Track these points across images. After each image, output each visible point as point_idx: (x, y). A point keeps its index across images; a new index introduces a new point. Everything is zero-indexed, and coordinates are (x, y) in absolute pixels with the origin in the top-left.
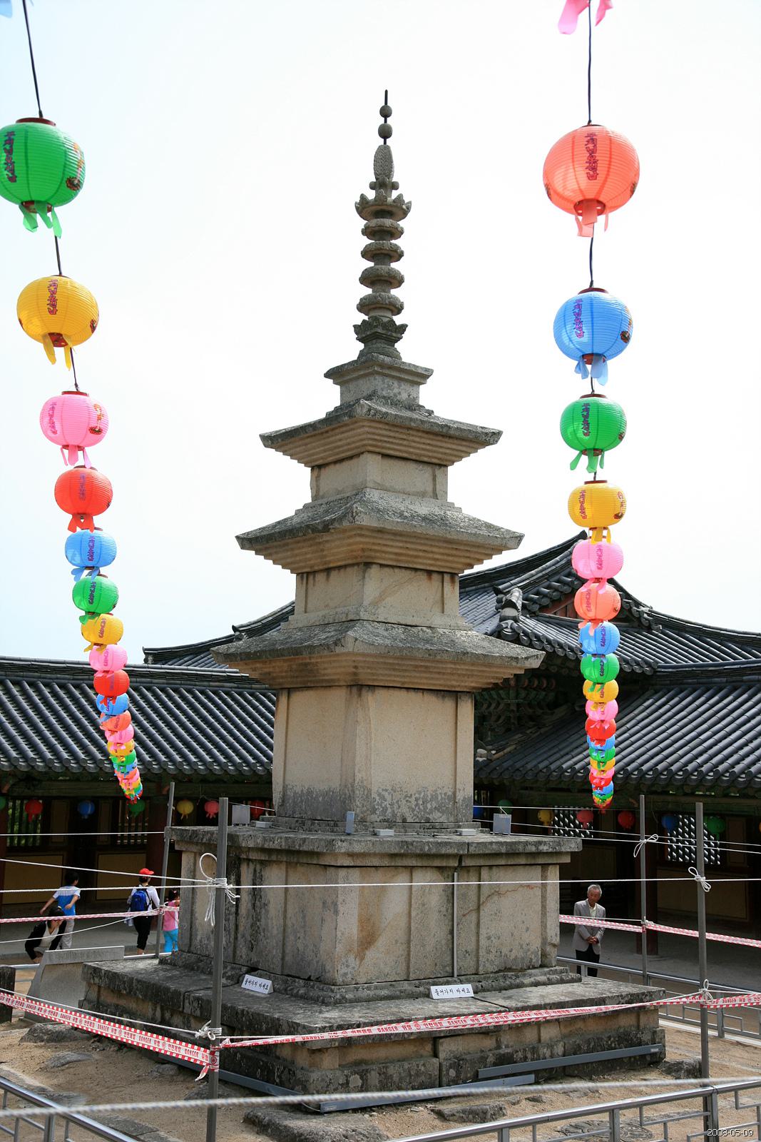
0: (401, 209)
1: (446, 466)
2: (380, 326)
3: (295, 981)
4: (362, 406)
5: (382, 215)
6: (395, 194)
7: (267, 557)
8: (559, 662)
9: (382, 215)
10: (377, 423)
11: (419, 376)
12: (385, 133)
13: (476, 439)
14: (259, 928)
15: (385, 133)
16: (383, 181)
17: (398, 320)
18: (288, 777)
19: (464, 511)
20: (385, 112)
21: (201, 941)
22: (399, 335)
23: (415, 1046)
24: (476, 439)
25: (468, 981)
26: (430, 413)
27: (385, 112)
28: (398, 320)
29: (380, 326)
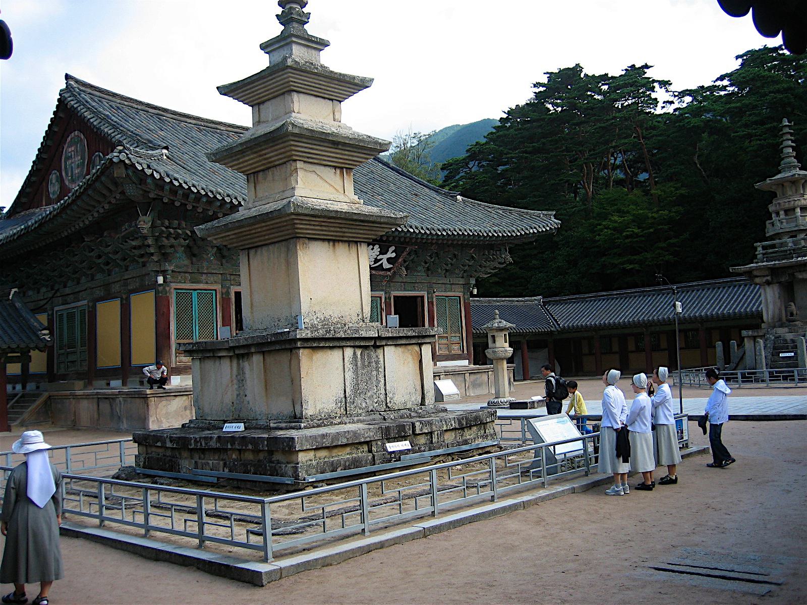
1: (340, 102)
13: (353, 85)
17: (305, 10)
18: (341, 353)
24: (353, 85)
28: (305, 10)
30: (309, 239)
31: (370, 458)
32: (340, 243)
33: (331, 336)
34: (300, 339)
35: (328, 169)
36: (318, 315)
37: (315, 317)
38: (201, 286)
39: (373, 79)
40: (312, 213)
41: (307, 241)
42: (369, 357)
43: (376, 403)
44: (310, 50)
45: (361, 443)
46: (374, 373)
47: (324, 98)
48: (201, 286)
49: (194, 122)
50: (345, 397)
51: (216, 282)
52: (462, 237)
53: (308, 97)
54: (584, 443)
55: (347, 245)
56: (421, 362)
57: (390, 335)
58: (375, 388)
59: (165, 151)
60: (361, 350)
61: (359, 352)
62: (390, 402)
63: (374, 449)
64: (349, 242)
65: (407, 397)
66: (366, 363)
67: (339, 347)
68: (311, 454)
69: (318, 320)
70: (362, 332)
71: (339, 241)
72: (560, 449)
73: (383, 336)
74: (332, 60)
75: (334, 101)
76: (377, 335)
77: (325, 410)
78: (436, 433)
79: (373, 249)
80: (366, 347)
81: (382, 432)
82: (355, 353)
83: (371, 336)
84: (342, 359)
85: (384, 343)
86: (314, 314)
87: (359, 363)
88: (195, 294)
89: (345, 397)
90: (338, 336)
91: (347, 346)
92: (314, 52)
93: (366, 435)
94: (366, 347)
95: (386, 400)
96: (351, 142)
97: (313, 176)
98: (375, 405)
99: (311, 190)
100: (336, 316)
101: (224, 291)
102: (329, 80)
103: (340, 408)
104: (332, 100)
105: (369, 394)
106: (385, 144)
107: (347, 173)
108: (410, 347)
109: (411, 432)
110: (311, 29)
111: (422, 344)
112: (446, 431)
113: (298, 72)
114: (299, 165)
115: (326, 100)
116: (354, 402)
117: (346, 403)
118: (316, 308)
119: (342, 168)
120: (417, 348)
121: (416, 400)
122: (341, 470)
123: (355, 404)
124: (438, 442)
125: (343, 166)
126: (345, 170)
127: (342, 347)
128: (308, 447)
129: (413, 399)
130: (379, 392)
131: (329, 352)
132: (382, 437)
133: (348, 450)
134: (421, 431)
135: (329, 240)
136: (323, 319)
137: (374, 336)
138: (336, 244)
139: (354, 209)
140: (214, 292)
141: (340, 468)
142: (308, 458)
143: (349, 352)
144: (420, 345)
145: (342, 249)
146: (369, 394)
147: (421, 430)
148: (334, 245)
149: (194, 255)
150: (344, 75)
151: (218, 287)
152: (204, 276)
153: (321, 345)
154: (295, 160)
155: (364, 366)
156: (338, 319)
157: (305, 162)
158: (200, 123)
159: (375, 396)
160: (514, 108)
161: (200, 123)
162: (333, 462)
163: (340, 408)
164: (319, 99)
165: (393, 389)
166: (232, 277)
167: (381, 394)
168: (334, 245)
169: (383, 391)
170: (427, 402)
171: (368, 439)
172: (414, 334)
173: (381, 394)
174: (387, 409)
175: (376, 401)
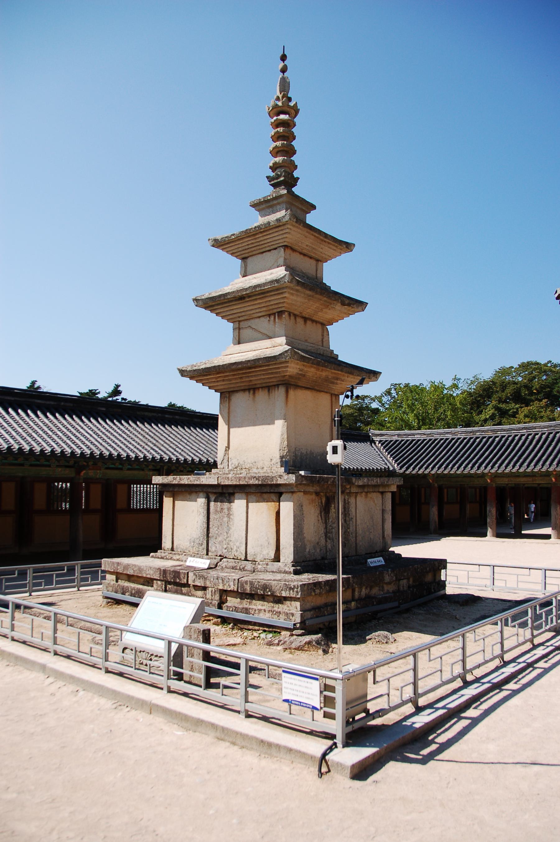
5: (285, 118)
6: (292, 104)
9: (285, 118)
14: (349, 533)
20: (284, 58)
21: (309, 552)
27: (284, 58)
29: (284, 176)
33: (177, 483)
46: (226, 519)
47: (270, 251)
53: (254, 258)
58: (225, 534)
60: (215, 496)
62: (237, 551)
76: (216, 483)
77: (181, 546)
78: (210, 589)
81: (160, 573)
93: (148, 572)
96: (248, 292)
98: (225, 551)
100: (250, 462)
104: (275, 249)
106: (281, 278)
109: (185, 581)
121: (268, 554)
125: (269, 313)
136: (237, 465)
137: (213, 483)
145: (262, 395)
146: (220, 539)
147: (194, 581)
148: (254, 393)
156: (251, 465)
159: (224, 542)
160: (296, 174)
164: (264, 254)
167: (231, 541)
168: (254, 393)
173: (231, 541)
175: (225, 546)
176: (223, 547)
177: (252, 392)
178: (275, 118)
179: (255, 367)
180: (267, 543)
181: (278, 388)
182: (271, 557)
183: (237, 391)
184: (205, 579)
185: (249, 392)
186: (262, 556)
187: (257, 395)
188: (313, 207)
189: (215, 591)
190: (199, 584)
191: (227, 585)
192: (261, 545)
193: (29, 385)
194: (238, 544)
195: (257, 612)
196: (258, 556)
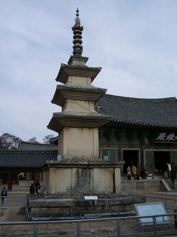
0: (81, 29)
2: (78, 50)
3: (81, 223)
4: (123, 189)
5: (78, 30)
7: (55, 104)
8: (125, 124)
9: (78, 30)
10: (75, 69)
11: (86, 59)
12: (77, 15)
15: (77, 15)
16: (78, 21)
18: (71, 171)
19: (95, 86)
20: (77, 11)
22: (81, 52)
23: (51, 193)
25: (96, 196)
26: (94, 86)
27: (77, 11)
29: (78, 50)
30: (70, 127)
31: (68, 213)
32: (85, 129)
33: (63, 163)
34: (50, 164)
35: (82, 101)
36: (72, 155)
37: (70, 156)
38: (111, 148)
39: (101, 68)
40: (64, 117)
41: (68, 128)
42: (85, 172)
43: (88, 191)
44: (81, 62)
45: (66, 207)
46: (88, 179)
47: (84, 77)
48: (111, 148)
49: (121, 98)
50: (71, 188)
51: (116, 147)
52: (128, 124)
53: (76, 77)
54: (118, 221)
55: (88, 129)
56: (114, 176)
57: (95, 164)
58: (88, 185)
59: (99, 107)
60: (82, 169)
61: (80, 170)
62: (95, 191)
63: (71, 210)
64: (89, 128)
65: (105, 190)
66: (84, 175)
67: (70, 168)
68: (38, 209)
69: (72, 157)
70: (80, 162)
71: (84, 128)
72: (143, 220)
73: (91, 164)
74: (89, 64)
75: (88, 78)
76: (87, 164)
77: (61, 192)
79: (172, 134)
80: (85, 168)
82: (78, 171)
83: (84, 164)
84: (71, 172)
85: (93, 167)
86: (70, 155)
87: (80, 175)
88: (109, 151)
89: (71, 188)
90: (67, 163)
91: (74, 168)
92: (82, 62)
94: (85, 168)
95: (93, 190)
97: (75, 104)
98: (87, 192)
99: (73, 109)
100: (81, 156)
101: (119, 150)
102: (82, 70)
103: (69, 192)
104: (87, 77)
105: (85, 187)
106: (104, 90)
107: (91, 102)
108: (108, 169)
110: (83, 55)
111: (116, 167)
112: (112, 205)
113: (67, 69)
114: (69, 100)
115: (84, 77)
116: (76, 190)
117: (72, 190)
118: (71, 153)
119: (89, 101)
120: (112, 169)
122: (52, 217)
123: (76, 191)
124: (107, 210)
126: (90, 101)
127: (71, 168)
128: (35, 206)
129: (108, 191)
130: (90, 187)
131: (65, 169)
132: (75, 205)
133: (58, 209)
134: (98, 204)
135: (79, 128)
136: (74, 157)
138: (83, 129)
139: (94, 115)
140: (115, 150)
141: (51, 216)
142: (35, 210)
143: (75, 170)
144: (114, 168)
145: (86, 131)
146: (85, 187)
148: (82, 129)
149: (108, 139)
150: (92, 68)
151: (117, 149)
152: (112, 145)
153: (63, 167)
154: (67, 99)
155: (82, 176)
157: (71, 99)
158: (123, 98)
161: (123, 98)
162: (48, 213)
163: (69, 192)
164: (81, 77)
165: (97, 186)
166: (122, 145)
167: (91, 187)
168: (82, 129)
169: (92, 186)
170: (116, 192)
171: (70, 206)
172: (108, 164)
173: (91, 187)
174: (94, 194)
175: (88, 190)
176: (87, 190)
177: (81, 129)
178: (75, 31)
179: (96, 120)
180: (110, 187)
181: (95, 129)
182: (111, 192)
183: (73, 127)
184: (104, 202)
185: (79, 129)
186: (107, 192)
187: (90, 131)
188: (106, 90)
189: (109, 206)
190: (101, 205)
191: (115, 202)
192: (107, 188)
193: (74, 23)
194: (96, 188)
195: (130, 210)
196: (106, 192)
